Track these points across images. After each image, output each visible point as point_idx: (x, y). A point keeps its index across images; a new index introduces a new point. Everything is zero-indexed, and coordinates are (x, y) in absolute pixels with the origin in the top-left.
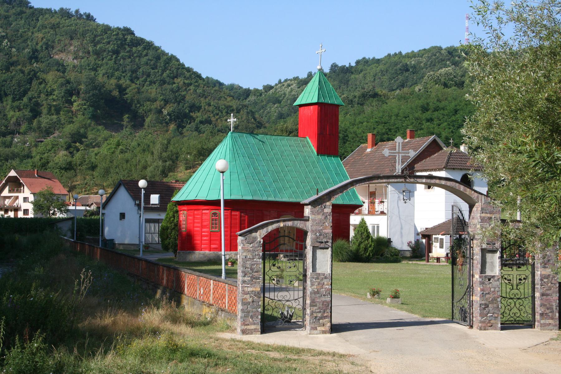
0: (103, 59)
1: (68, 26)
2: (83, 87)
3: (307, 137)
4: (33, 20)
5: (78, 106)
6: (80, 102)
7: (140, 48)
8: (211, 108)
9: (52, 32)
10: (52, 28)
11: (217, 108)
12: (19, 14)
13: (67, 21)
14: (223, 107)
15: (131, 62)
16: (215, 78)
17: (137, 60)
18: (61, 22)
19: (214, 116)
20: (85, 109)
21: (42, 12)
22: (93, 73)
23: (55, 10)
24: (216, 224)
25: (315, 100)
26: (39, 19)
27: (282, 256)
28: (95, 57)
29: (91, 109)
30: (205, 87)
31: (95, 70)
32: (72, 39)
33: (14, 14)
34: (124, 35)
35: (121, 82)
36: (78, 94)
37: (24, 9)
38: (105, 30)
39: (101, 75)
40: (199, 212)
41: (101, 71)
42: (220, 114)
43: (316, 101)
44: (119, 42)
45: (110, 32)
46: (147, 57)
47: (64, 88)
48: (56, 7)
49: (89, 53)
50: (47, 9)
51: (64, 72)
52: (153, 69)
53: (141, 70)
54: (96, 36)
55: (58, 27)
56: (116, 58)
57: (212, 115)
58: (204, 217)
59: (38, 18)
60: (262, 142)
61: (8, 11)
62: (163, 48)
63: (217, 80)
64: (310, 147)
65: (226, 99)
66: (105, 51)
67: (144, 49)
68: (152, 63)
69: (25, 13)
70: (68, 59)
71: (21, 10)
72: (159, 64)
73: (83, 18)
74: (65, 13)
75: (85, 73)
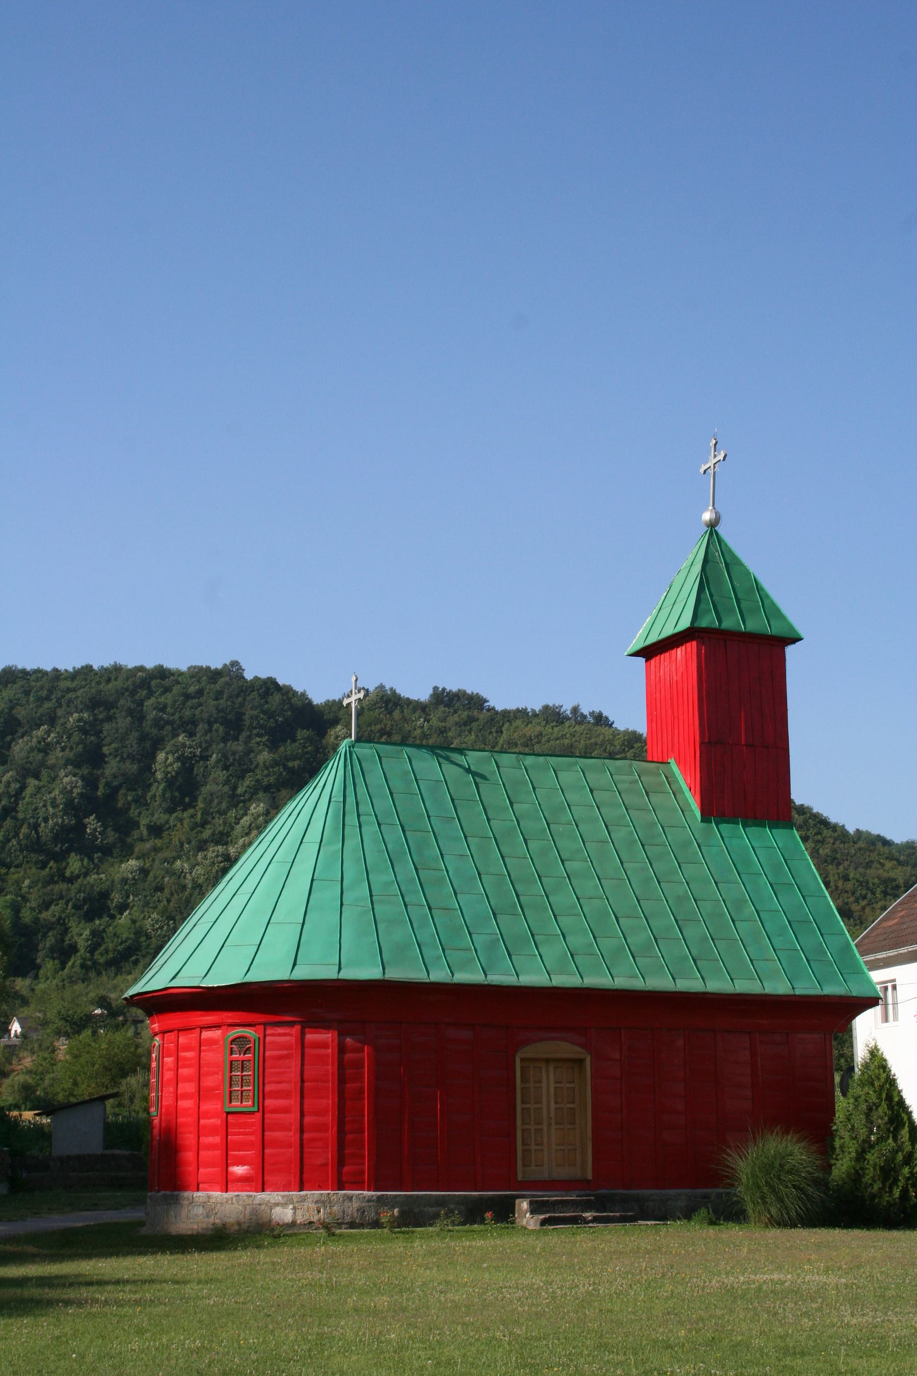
1: (557, 739)
3: (672, 761)
4: (491, 733)
8: (849, 886)
10: (527, 746)
11: (864, 884)
12: (465, 724)
13: (556, 729)
14: (876, 881)
16: (875, 832)
18: (544, 733)
19: (857, 901)
21: (508, 716)
23: (533, 711)
26: (504, 729)
27: (525, 1205)
30: (838, 842)
33: (457, 724)
37: (476, 713)
38: (629, 741)
42: (869, 896)
45: (639, 744)
48: (535, 705)
50: (518, 711)
55: (538, 743)
57: (852, 899)
58: (208, 1056)
59: (501, 727)
60: (474, 774)
61: (444, 720)
63: (879, 836)
65: (883, 865)
69: (478, 719)
71: (468, 716)
73: (589, 722)
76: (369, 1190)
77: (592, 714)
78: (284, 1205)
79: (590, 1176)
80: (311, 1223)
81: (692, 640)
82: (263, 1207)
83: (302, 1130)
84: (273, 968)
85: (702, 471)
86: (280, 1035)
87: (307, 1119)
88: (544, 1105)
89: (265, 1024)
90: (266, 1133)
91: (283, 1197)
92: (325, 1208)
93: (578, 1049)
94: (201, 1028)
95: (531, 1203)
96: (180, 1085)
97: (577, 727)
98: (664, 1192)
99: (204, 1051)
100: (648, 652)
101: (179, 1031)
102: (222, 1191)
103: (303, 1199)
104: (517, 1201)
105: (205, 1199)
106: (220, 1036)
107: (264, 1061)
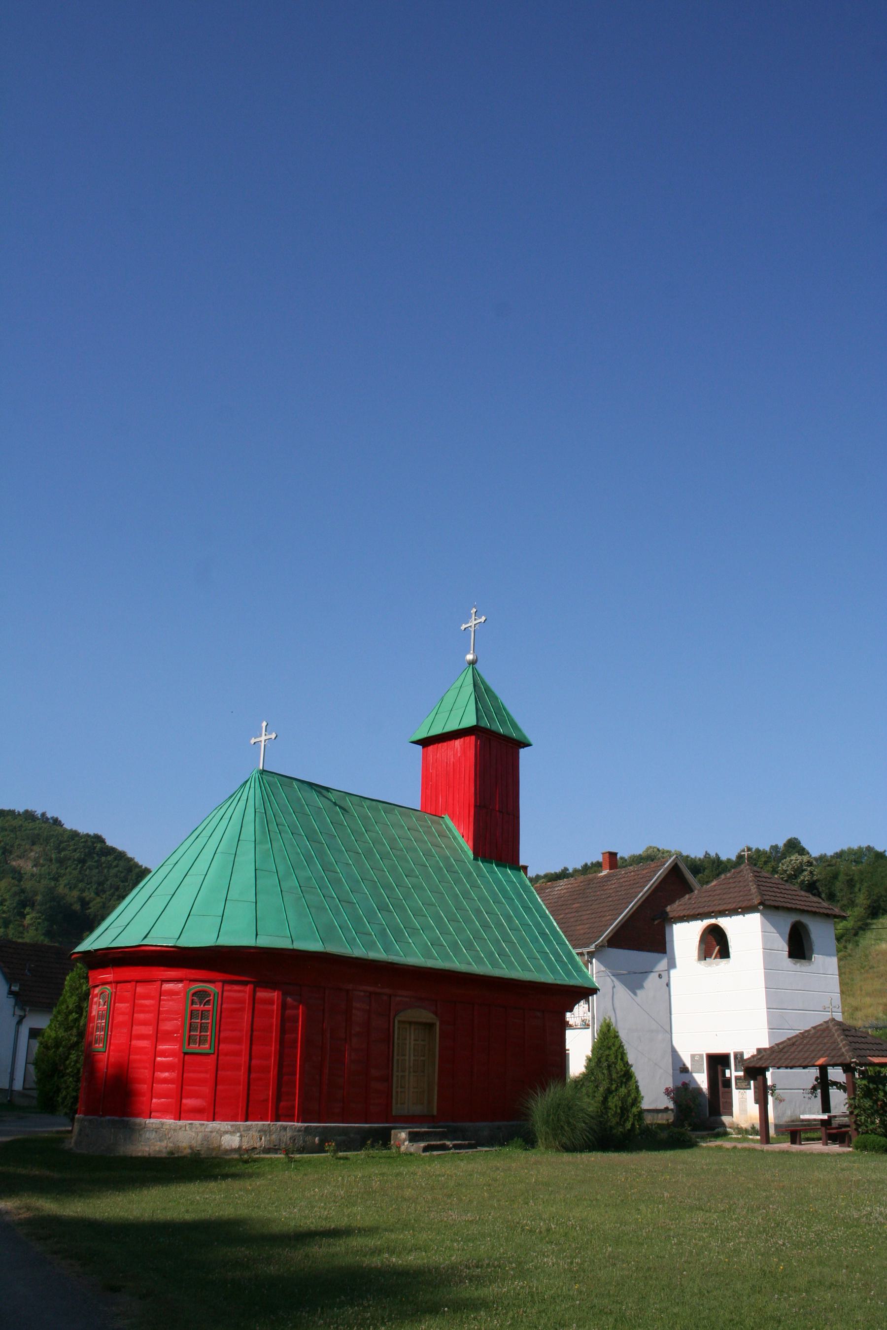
0: (66, 868)
2: (39, 898)
5: (32, 919)
6: (34, 915)
7: (110, 858)
9: (12, 835)
15: (99, 873)
17: (106, 871)
20: (39, 924)
22: (53, 883)
24: (203, 1028)
25: (470, 721)
27: (403, 1135)
28: (58, 865)
29: (46, 923)
31: (56, 879)
32: (33, 843)
34: (93, 843)
35: (84, 895)
36: (33, 906)
39: (62, 886)
40: (152, 988)
41: (63, 882)
43: (474, 723)
44: (87, 850)
46: (117, 869)
47: (17, 898)
48: (20, 809)
49: (51, 860)
50: (10, 811)
51: (20, 880)
52: (123, 882)
53: (109, 883)
54: (61, 842)
56: (82, 867)
58: (168, 1005)
60: (340, 807)
62: (136, 860)
64: (455, 838)
66: (69, 859)
67: (115, 859)
68: (123, 875)
70: (27, 866)
72: (129, 877)
74: (29, 816)
75: (44, 882)
76: (298, 1122)
77: (52, 818)
78: (232, 1133)
79: (435, 1112)
80: (254, 1148)
81: (471, 735)
82: (214, 1134)
83: (250, 1070)
84: (201, 937)
85: (463, 628)
86: (236, 991)
87: (254, 1062)
88: (407, 1058)
89: (224, 982)
90: (219, 1072)
91: (232, 1126)
92: (266, 1135)
93: (432, 1016)
94: (137, 982)
95: (410, 1133)
96: (135, 1027)
97: (43, 825)
98: (477, 1124)
99: (164, 1000)
100: (425, 743)
101: (137, 982)
102: (175, 1119)
103: (249, 1129)
104: (393, 1132)
105: (158, 1126)
106: (176, 989)
107: (221, 1012)
